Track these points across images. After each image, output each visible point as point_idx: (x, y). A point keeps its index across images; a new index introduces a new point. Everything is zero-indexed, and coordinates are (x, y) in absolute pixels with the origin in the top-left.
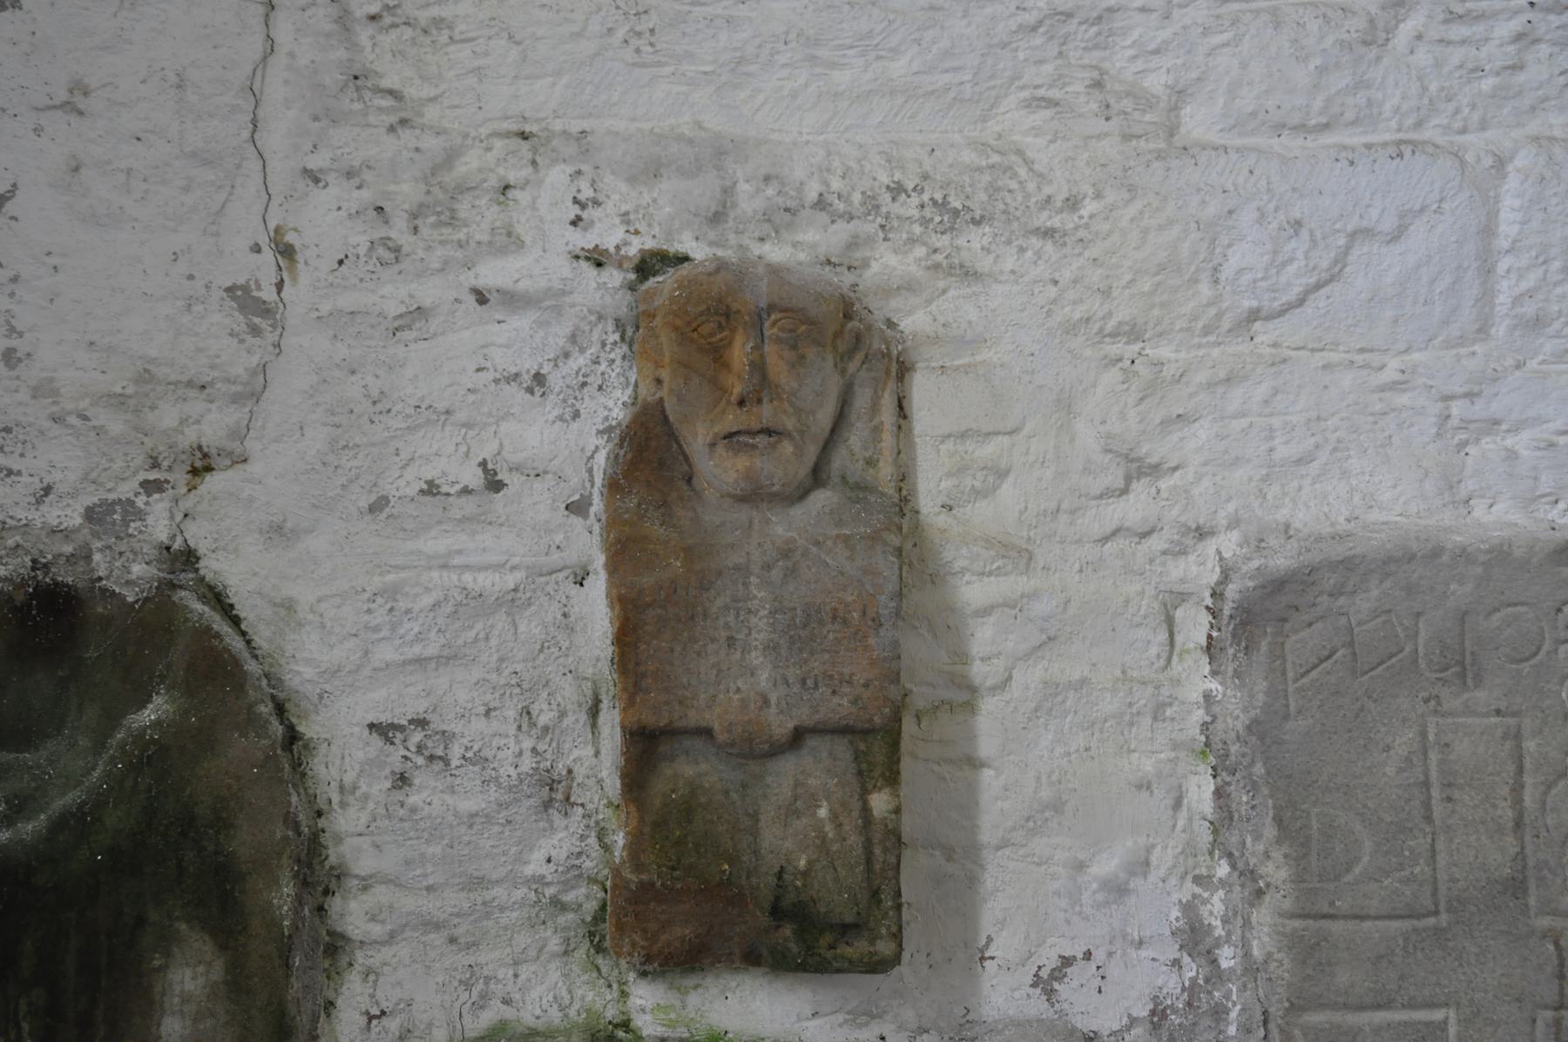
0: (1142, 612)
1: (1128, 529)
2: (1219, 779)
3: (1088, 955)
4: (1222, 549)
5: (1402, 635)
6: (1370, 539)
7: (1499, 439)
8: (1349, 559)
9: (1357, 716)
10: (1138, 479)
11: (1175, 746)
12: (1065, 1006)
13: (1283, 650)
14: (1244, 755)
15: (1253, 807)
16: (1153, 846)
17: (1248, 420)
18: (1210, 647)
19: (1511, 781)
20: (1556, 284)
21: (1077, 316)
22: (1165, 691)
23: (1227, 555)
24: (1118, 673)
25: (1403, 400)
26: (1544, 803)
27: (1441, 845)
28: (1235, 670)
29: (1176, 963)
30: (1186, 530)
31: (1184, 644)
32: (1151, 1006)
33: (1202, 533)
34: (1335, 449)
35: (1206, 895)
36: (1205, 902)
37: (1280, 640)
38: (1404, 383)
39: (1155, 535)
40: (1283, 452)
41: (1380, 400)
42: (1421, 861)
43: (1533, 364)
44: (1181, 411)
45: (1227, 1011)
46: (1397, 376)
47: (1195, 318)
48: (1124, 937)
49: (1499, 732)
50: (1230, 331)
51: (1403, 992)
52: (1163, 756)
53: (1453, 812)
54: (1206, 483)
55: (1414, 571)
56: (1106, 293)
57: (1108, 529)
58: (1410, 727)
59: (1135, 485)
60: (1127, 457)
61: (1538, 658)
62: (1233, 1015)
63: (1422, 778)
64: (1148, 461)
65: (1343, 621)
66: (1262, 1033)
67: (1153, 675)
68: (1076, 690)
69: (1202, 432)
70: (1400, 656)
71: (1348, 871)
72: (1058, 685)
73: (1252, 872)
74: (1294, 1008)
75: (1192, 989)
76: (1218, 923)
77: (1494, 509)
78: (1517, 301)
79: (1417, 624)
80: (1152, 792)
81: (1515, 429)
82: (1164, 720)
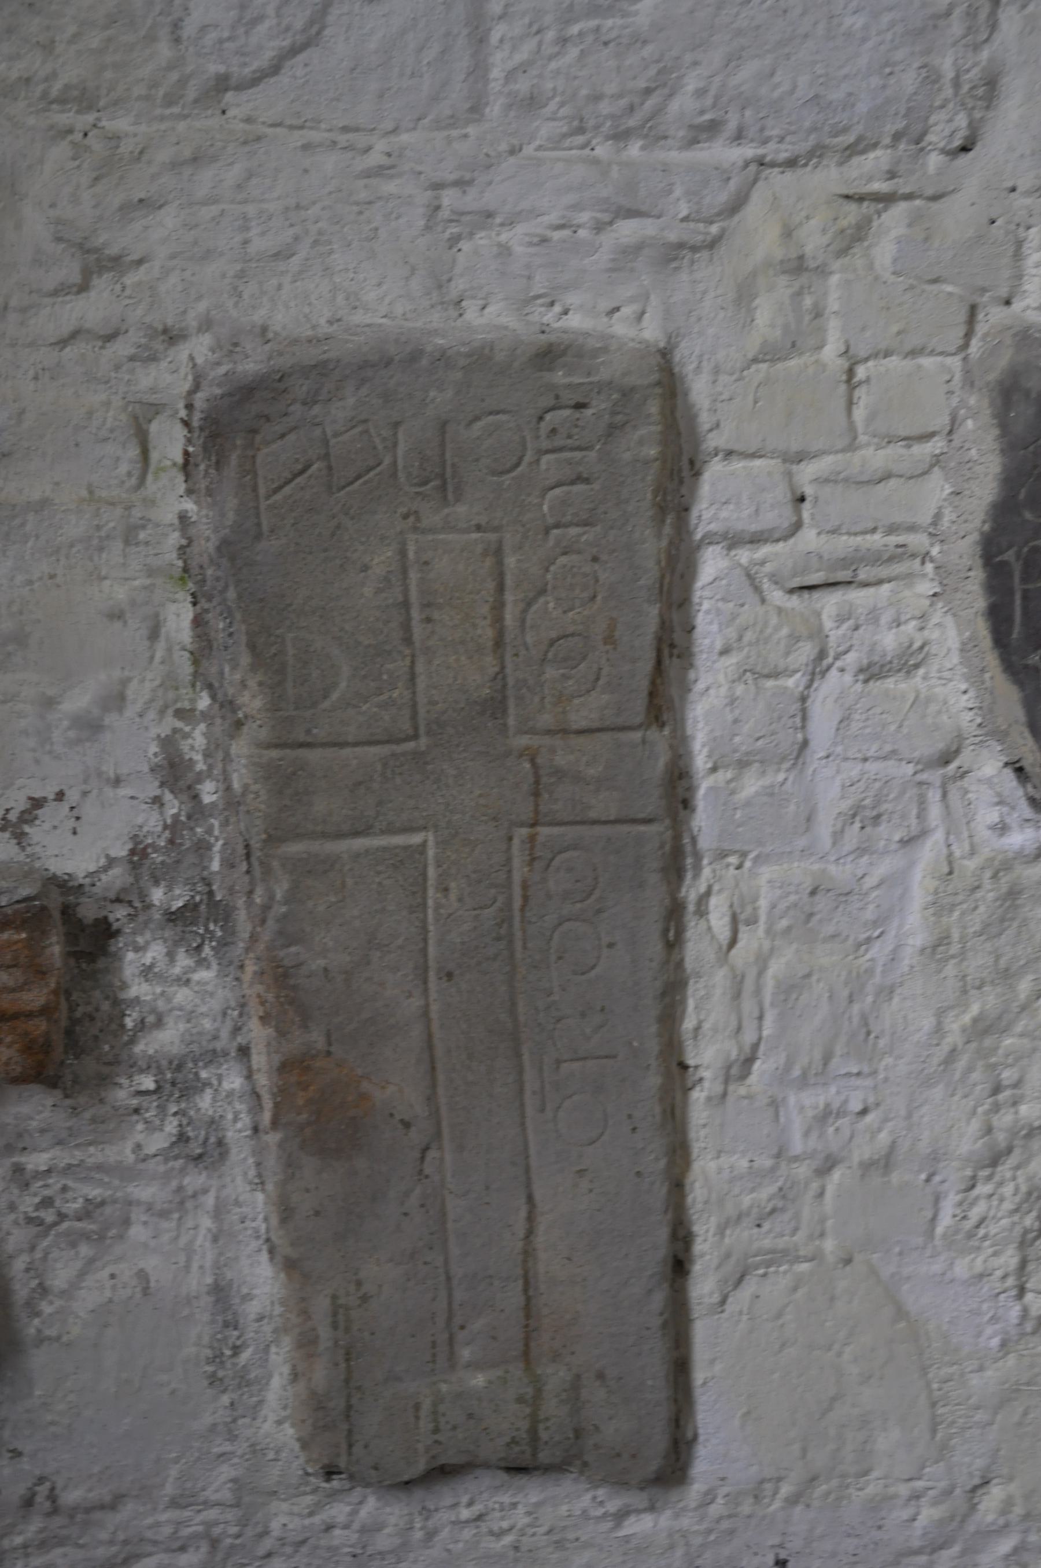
0: (108, 425)
1: (88, 331)
2: (198, 607)
3: (60, 796)
4: (195, 355)
5: (380, 447)
6: (347, 341)
7: (493, 234)
8: (324, 363)
9: (333, 535)
10: (100, 275)
11: (151, 572)
12: (38, 849)
13: (254, 462)
14: (218, 579)
15: (231, 635)
16: (129, 680)
17: (221, 206)
18: (187, 466)
19: (491, 599)
20: (551, 58)
21: (14, 75)
22: (137, 513)
23: (200, 360)
24: (84, 493)
25: (390, 187)
26: (523, 621)
27: (420, 668)
28: (207, 488)
29: (157, 801)
30: (152, 333)
31: (160, 461)
32: (130, 846)
33: (172, 337)
34: (316, 242)
35: (187, 729)
36: (186, 736)
37: (250, 453)
38: (389, 168)
39: (120, 338)
40: (259, 244)
41: (366, 186)
42: (400, 684)
43: (529, 150)
44: (142, 195)
45: (209, 847)
46: (384, 161)
47: (154, 85)
48: (100, 774)
49: (479, 549)
50: (196, 101)
51: (381, 818)
52: (137, 583)
53: (433, 632)
54: (173, 279)
55: (391, 377)
56: (48, 48)
57: (66, 330)
58: (389, 545)
59: (96, 281)
60: (81, 246)
61: (520, 469)
62: (218, 846)
63: (401, 599)
64: (107, 252)
65: (317, 432)
66: (244, 867)
67: (124, 496)
68: (36, 512)
69: (169, 219)
70: (379, 469)
71: (325, 697)
72: (14, 506)
73: (231, 702)
74: (272, 840)
75: (174, 827)
76: (198, 757)
77: (487, 310)
78: (510, 76)
79: (395, 434)
80: (125, 622)
81: (509, 223)
82: (137, 544)
